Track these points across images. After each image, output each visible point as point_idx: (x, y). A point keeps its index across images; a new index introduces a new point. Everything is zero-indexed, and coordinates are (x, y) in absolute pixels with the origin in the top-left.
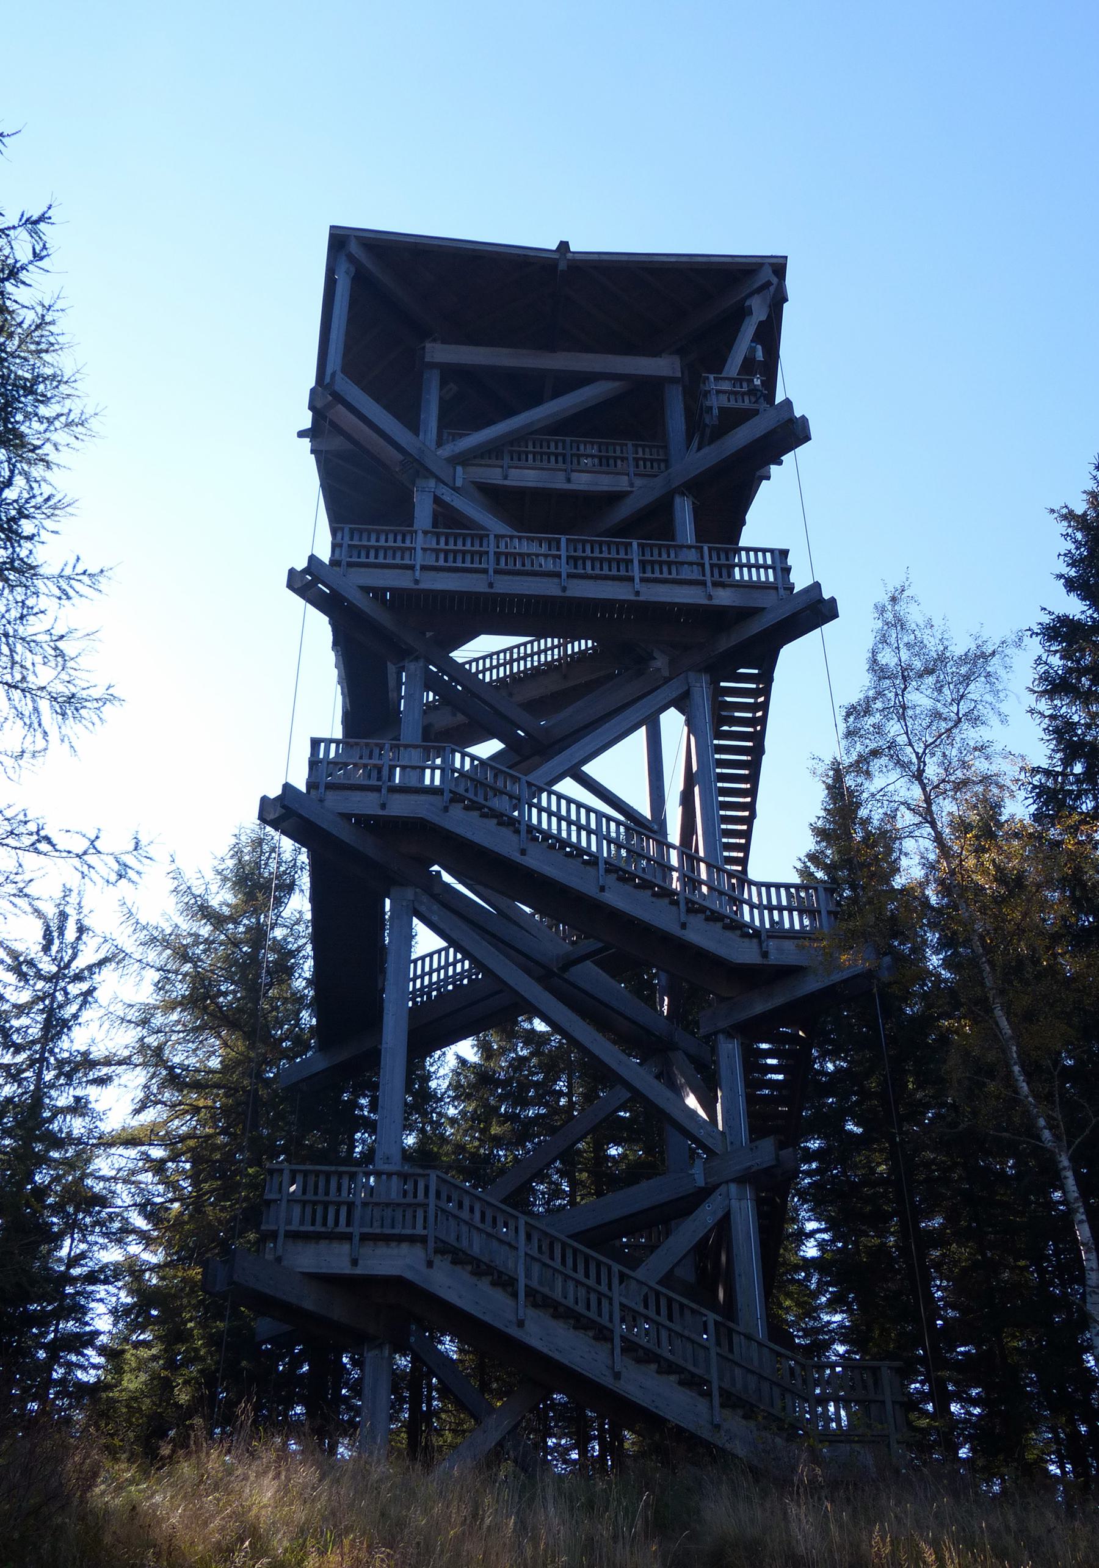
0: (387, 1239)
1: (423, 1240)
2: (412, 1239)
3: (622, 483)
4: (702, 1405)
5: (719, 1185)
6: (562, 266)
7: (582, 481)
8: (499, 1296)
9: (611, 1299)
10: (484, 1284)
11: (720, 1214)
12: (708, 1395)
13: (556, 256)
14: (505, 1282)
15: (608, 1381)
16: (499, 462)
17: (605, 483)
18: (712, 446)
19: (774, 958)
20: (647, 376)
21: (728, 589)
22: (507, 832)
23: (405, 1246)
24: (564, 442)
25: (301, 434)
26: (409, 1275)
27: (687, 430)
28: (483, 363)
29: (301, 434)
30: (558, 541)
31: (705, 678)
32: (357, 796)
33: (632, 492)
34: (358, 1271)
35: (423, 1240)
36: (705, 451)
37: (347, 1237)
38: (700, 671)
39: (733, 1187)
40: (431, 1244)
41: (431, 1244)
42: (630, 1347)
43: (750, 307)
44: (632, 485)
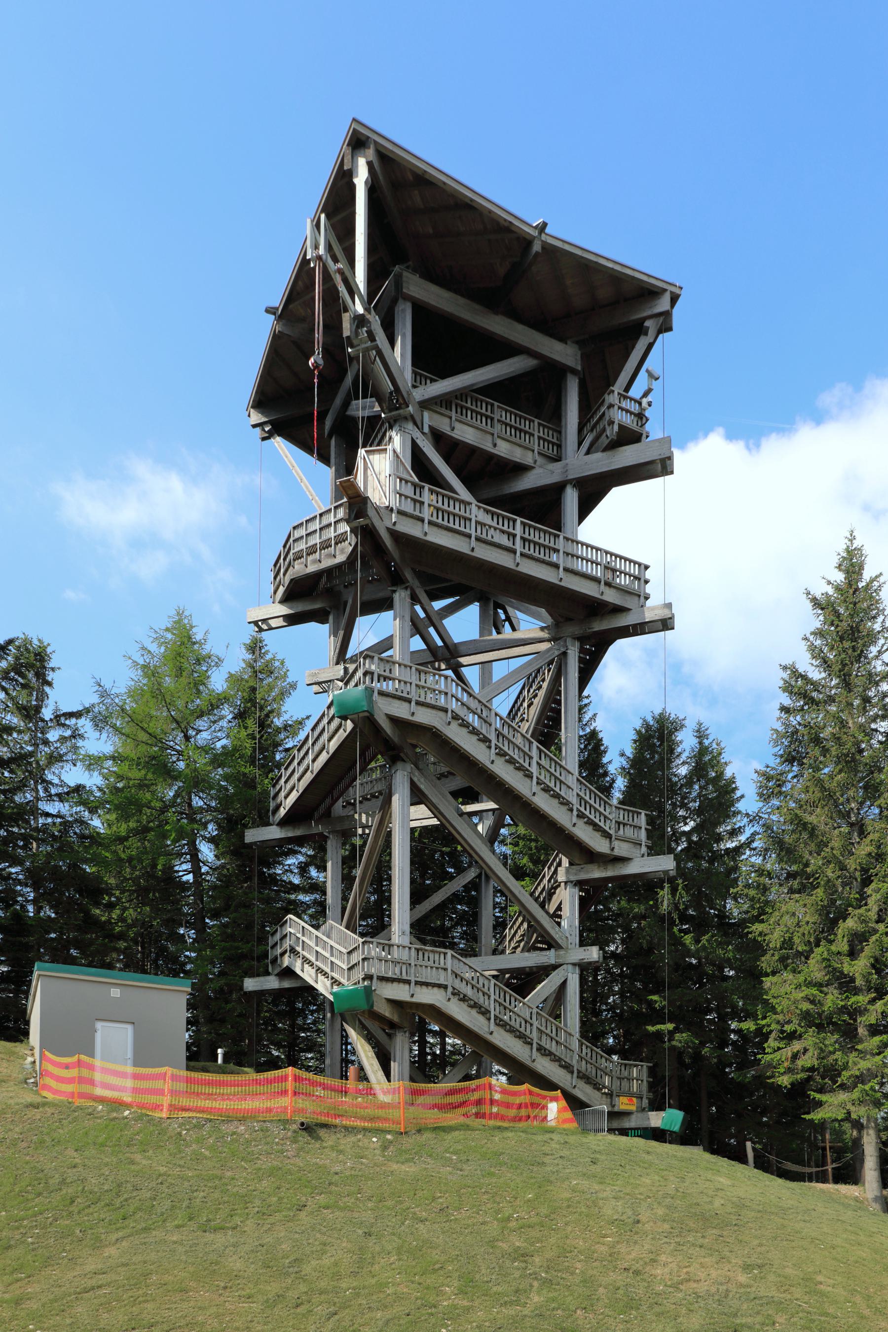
0: (427, 984)
1: (445, 987)
2: (439, 986)
3: (527, 458)
4: (569, 1076)
5: (561, 965)
6: (537, 247)
7: (503, 449)
8: (481, 1019)
9: (531, 1025)
10: (474, 1012)
11: (563, 979)
12: (572, 1072)
13: (535, 233)
14: (485, 1012)
15: (528, 1062)
16: (448, 412)
17: (517, 455)
18: (605, 454)
19: (617, 852)
20: (555, 360)
21: (612, 589)
22: (482, 746)
23: (436, 989)
24: (492, 405)
25: (270, 311)
26: (438, 1004)
27: (579, 424)
28: (446, 309)
29: (270, 311)
30: (514, 521)
31: (577, 644)
32: (397, 703)
33: (533, 468)
34: (414, 1000)
35: (445, 987)
36: (597, 456)
37: (408, 982)
38: (574, 638)
39: (570, 967)
40: (450, 990)
41: (450, 990)
42: (540, 1049)
43: (648, 328)
44: (535, 462)
